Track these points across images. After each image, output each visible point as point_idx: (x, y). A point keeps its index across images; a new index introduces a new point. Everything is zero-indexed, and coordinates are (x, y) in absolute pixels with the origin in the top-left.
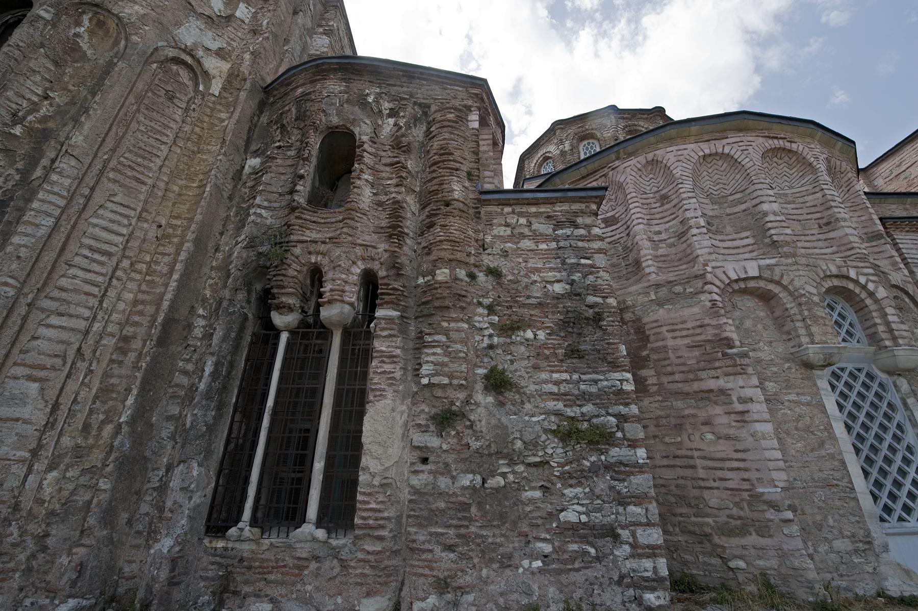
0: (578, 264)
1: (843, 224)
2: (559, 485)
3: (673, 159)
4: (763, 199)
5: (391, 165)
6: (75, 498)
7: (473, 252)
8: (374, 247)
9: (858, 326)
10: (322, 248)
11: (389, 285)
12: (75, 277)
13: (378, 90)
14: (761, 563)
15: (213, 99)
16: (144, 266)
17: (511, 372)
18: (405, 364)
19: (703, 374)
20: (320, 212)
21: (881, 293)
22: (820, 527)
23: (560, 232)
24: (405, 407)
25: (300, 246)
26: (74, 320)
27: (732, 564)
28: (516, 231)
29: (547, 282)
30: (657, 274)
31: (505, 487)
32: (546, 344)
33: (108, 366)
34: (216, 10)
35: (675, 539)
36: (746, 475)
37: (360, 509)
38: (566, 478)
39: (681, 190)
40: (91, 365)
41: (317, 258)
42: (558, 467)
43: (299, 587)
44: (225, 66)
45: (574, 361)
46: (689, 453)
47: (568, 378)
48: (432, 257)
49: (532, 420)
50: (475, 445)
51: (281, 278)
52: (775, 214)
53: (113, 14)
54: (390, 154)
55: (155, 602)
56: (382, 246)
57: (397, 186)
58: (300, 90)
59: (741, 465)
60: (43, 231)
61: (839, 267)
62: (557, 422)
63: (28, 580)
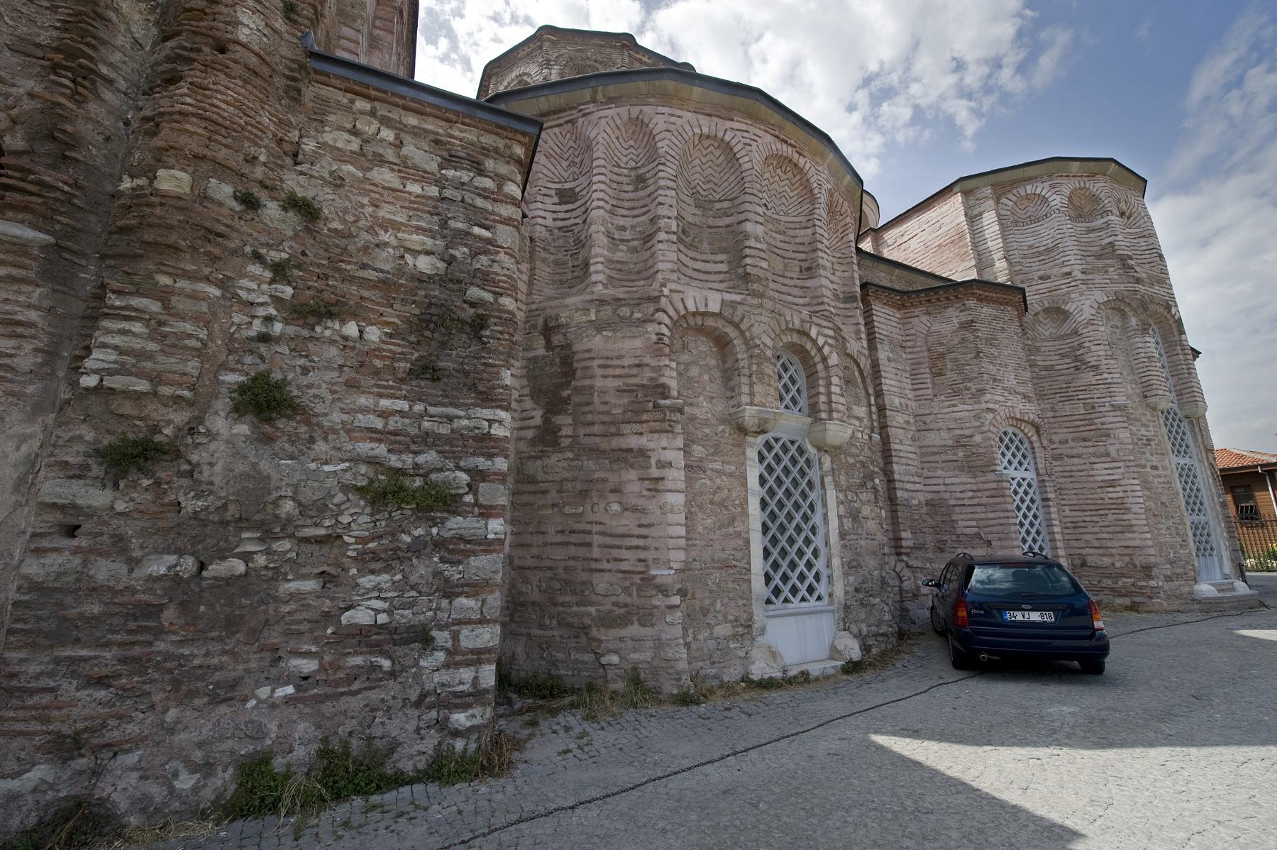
0: (468, 234)
1: (822, 272)
2: (354, 571)
3: (661, 126)
4: (750, 216)
7: (263, 158)
9: (805, 393)
11: (30, 172)
14: (635, 656)
17: (298, 387)
19: (626, 429)
21: (834, 360)
22: (705, 612)
23: (450, 173)
24: (36, 428)
27: (604, 660)
28: (369, 149)
29: (408, 250)
30: (605, 286)
31: (246, 574)
32: (379, 350)
35: (549, 633)
36: (643, 555)
38: (367, 561)
39: (661, 174)
42: (356, 543)
45: (423, 383)
46: (588, 527)
47: (406, 408)
48: (157, 142)
49: (322, 470)
50: (191, 504)
52: (757, 239)
59: (640, 542)
61: (803, 321)
62: (371, 474)
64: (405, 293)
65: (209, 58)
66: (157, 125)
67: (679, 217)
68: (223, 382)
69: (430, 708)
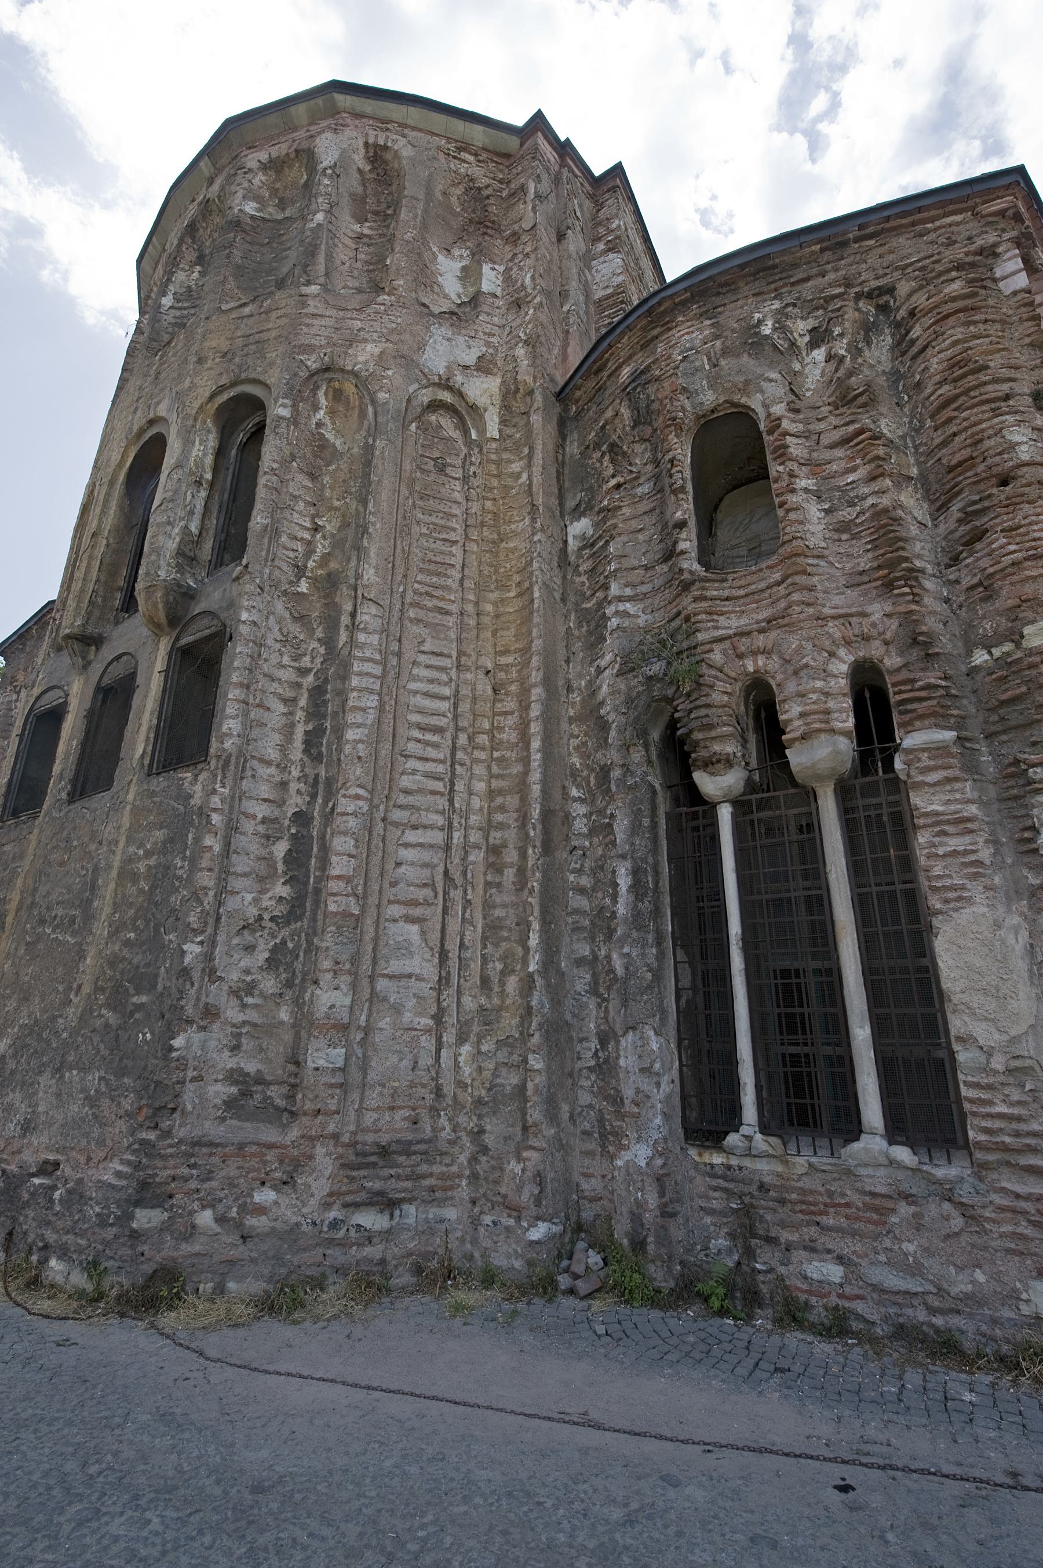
5: (845, 441)
6: (498, 1081)
8: (863, 615)
10: (760, 641)
11: (913, 681)
12: (414, 772)
13: (777, 305)
15: (494, 445)
16: (485, 737)
18: (993, 833)
20: (730, 577)
25: (717, 648)
26: (429, 833)
33: (485, 893)
34: (454, 297)
37: (975, 1114)
40: (465, 892)
41: (755, 662)
43: (887, 1243)
44: (493, 384)
51: (703, 712)
53: (348, 372)
54: (834, 420)
55: (650, 1239)
56: (877, 610)
57: (874, 479)
58: (626, 372)
60: (371, 717)
63: (477, 1191)
65: (1002, 497)
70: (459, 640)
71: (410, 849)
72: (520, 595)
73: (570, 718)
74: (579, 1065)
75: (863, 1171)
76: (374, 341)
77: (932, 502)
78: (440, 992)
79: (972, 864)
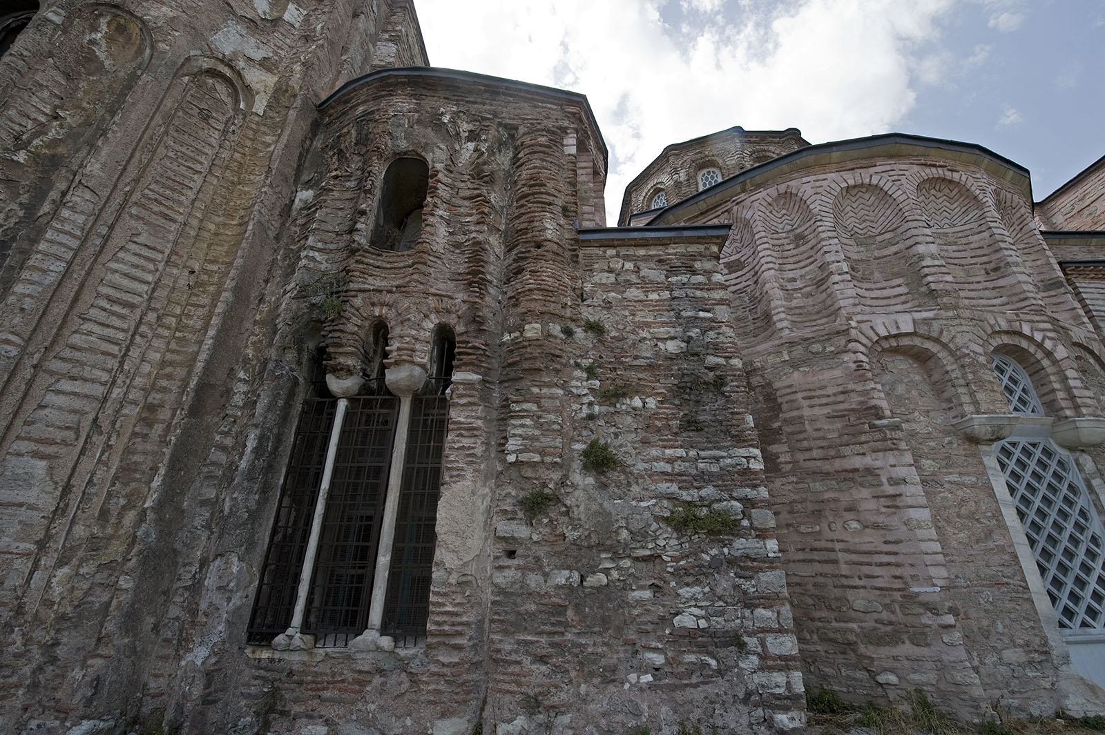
2: (673, 584)
4: (919, 239)
5: (471, 198)
6: (90, 599)
7: (569, 303)
9: (1033, 392)
10: (388, 298)
11: (468, 342)
12: (90, 333)
13: (455, 109)
14: (916, 677)
15: (257, 119)
18: (488, 438)
19: (846, 451)
20: (385, 254)
21: (1061, 352)
23: (674, 279)
24: (487, 490)
27: (882, 678)
28: (621, 278)
29: (659, 339)
31: (607, 585)
34: (260, 12)
35: (812, 648)
36: (898, 572)
38: (681, 575)
40: (109, 439)
42: (672, 561)
43: (360, 706)
44: (271, 80)
45: (691, 434)
46: (830, 545)
48: (520, 310)
49: (640, 505)
50: (572, 535)
51: (338, 334)
52: (933, 257)
53: (136, 17)
56: (460, 296)
57: (478, 223)
58: (361, 109)
60: (51, 279)
61: (1010, 321)
64: (664, 370)
66: (517, 300)
67: (847, 258)
68: (574, 450)
69: (756, 705)
70: (176, 243)
71: (61, 396)
72: (240, 225)
73: (255, 321)
74: (179, 584)
75: (359, 656)
76: (171, 7)
77: (507, 246)
78: (52, 520)
79: (470, 455)
